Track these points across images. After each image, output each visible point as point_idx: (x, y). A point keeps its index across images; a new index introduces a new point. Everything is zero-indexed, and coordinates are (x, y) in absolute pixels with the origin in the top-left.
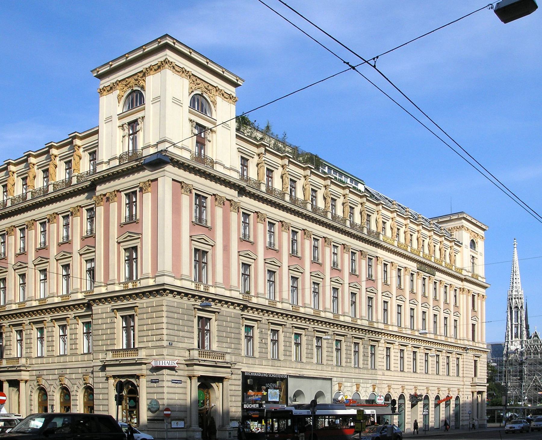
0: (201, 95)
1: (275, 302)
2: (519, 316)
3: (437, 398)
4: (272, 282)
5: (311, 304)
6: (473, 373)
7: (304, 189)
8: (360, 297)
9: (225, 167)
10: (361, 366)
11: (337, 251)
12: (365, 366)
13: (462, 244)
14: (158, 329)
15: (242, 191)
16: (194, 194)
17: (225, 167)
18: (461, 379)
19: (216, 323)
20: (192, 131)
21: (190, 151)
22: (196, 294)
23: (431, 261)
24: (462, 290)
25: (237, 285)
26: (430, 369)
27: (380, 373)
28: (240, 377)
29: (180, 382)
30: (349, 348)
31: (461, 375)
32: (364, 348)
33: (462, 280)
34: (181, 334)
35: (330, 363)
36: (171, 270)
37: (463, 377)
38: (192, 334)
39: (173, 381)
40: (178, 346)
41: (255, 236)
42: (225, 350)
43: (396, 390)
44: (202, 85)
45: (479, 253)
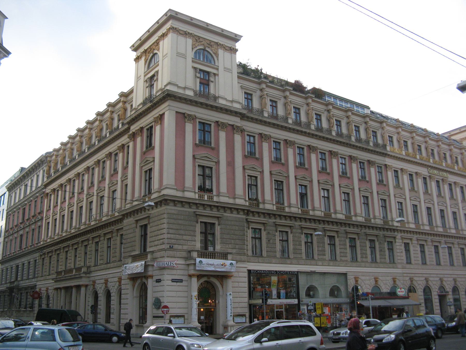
0: (204, 50)
1: (351, 217)
3: (442, 288)
7: (383, 137)
10: (378, 260)
12: (383, 260)
14: (152, 232)
15: (243, 117)
16: (198, 122)
19: (219, 227)
20: (196, 75)
21: (239, 103)
22: (197, 202)
24: (351, 158)
27: (399, 266)
28: (246, 274)
29: (181, 281)
32: (380, 243)
34: (185, 237)
35: (343, 259)
38: (194, 237)
39: (173, 281)
40: (179, 248)
42: (230, 251)
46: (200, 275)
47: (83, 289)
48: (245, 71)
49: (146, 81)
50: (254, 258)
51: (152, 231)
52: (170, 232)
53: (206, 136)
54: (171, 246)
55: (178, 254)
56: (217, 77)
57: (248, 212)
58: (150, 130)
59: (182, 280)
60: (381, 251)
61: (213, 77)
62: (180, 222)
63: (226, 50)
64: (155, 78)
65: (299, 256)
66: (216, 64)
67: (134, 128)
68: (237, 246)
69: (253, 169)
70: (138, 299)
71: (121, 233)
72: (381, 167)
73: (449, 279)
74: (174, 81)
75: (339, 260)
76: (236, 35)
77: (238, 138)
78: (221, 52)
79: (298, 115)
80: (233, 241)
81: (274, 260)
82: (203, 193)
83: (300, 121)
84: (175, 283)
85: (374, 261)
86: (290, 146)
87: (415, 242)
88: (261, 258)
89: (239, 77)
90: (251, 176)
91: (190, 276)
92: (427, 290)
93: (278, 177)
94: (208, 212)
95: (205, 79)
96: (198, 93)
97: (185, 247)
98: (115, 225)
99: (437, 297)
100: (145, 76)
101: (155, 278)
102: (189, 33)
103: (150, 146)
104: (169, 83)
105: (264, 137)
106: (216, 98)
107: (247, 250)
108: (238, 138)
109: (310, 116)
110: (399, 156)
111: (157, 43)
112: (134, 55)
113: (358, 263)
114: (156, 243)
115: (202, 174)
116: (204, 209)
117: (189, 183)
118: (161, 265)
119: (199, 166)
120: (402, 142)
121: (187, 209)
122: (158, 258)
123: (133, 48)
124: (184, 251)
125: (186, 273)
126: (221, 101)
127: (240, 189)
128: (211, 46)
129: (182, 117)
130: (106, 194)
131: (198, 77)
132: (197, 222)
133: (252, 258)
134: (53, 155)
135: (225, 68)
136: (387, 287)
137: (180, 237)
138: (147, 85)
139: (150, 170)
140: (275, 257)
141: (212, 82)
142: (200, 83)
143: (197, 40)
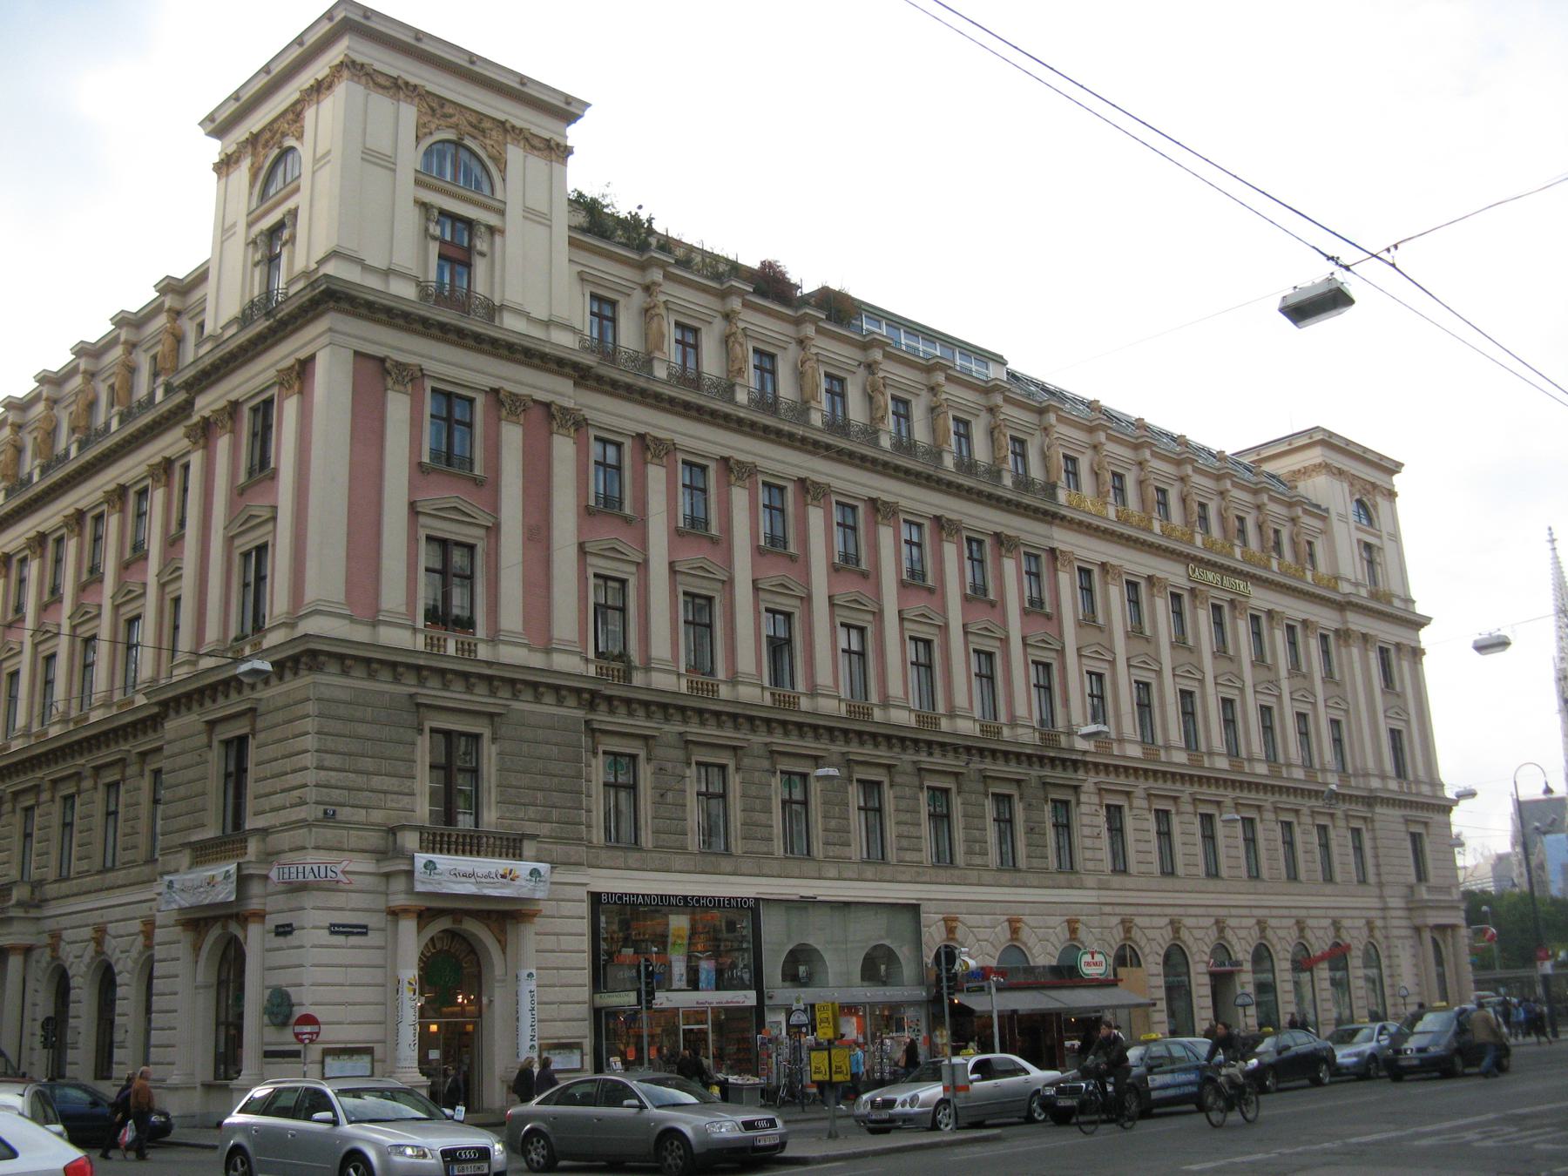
0: (458, 144)
4: (987, 678)
6: (1412, 870)
7: (1045, 457)
9: (366, 268)
10: (1022, 862)
11: (920, 534)
12: (1036, 863)
13: (1327, 510)
15: (582, 376)
17: (366, 268)
19: (494, 749)
21: (573, 329)
22: (422, 662)
25: (966, 705)
27: (1090, 881)
28: (584, 908)
29: (362, 930)
31: (1372, 878)
32: (1029, 807)
33: (1342, 606)
34: (376, 782)
35: (908, 856)
36: (341, 597)
38: (408, 782)
39: (335, 929)
40: (355, 818)
41: (804, 541)
42: (529, 828)
48: (595, 224)
49: (254, 242)
51: (266, 757)
52: (326, 764)
54: (330, 809)
55: (353, 838)
56: (498, 238)
57: (592, 699)
58: (265, 410)
59: (365, 927)
60: (1030, 831)
61: (486, 237)
62: (363, 729)
63: (533, 147)
64: (286, 235)
66: (499, 195)
67: (207, 403)
68: (555, 814)
69: (614, 553)
70: (213, 992)
74: (350, 246)
76: (569, 99)
77: (564, 448)
80: (539, 794)
81: (678, 861)
84: (341, 939)
85: (1009, 863)
87: (1139, 802)
88: (637, 855)
89: (572, 242)
90: (606, 578)
91: (395, 914)
92: (1175, 959)
94: (456, 695)
95: (459, 244)
96: (432, 290)
97: (377, 816)
99: (1206, 979)
100: (250, 225)
102: (407, 84)
103: (261, 467)
104: (334, 254)
105: (652, 446)
106: (492, 311)
107: (589, 826)
108: (564, 448)
110: (1096, 522)
111: (295, 113)
112: (214, 149)
113: (957, 872)
115: (438, 566)
116: (446, 687)
117: (393, 596)
118: (293, 875)
119: (429, 538)
120: (1108, 477)
121: (384, 685)
122: (284, 852)
125: (381, 903)
127: (566, 619)
128: (483, 131)
129: (376, 372)
130: (105, 632)
131: (434, 238)
132: (420, 731)
133: (604, 855)
135: (527, 210)
136: (1050, 948)
137: (360, 780)
139: (262, 550)
140: (683, 850)
141: (482, 254)
142: (441, 256)
143: (433, 110)
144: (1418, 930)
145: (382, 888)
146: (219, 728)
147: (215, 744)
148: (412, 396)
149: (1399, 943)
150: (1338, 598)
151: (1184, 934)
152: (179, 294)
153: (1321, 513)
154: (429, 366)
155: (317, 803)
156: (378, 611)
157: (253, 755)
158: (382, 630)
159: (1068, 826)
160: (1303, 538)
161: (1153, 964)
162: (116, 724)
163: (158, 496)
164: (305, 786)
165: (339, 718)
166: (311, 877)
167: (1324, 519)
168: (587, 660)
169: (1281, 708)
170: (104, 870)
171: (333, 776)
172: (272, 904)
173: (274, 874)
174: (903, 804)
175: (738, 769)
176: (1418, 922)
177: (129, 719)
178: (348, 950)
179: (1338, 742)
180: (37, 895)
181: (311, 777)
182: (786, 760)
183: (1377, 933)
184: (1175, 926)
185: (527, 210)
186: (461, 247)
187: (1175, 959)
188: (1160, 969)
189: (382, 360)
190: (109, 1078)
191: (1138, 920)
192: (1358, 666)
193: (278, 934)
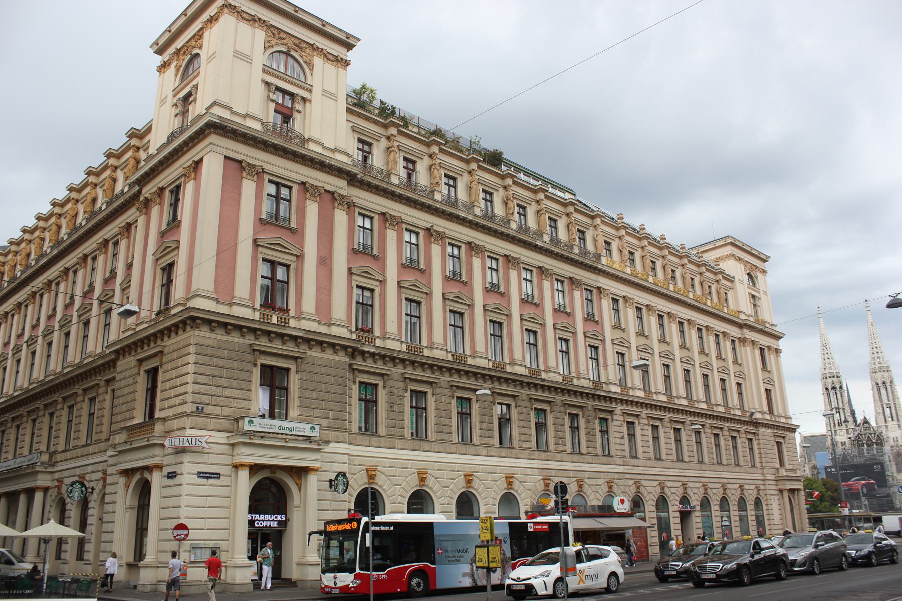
1: (538, 372)
2: (890, 394)
4: (497, 337)
5: (588, 374)
6: (778, 461)
7: (595, 241)
8: (713, 379)
10: (584, 450)
11: (532, 276)
12: (591, 450)
15: (352, 179)
18: (760, 471)
19: (297, 377)
20: (268, 96)
22: (257, 326)
23: (648, 282)
26: (741, 459)
29: (217, 476)
30: (560, 421)
31: (758, 465)
32: (587, 421)
33: (741, 326)
34: (228, 392)
35: (525, 445)
36: (212, 289)
37: (762, 468)
38: (247, 393)
39: (201, 475)
40: (215, 412)
43: (650, 490)
44: (290, 41)
45: (761, 293)
46: (256, 465)
47: (38, 496)
48: (359, 103)
49: (176, 105)
50: (362, 437)
51: (167, 378)
52: (199, 381)
53: (282, 207)
54: (200, 406)
55: (212, 423)
56: (307, 104)
57: (354, 352)
58: (177, 191)
59: (219, 474)
60: (588, 434)
61: (302, 103)
62: (221, 362)
63: (329, 59)
64: (192, 99)
65: (446, 437)
67: (148, 190)
68: (331, 414)
69: (367, 275)
70: (135, 513)
71: (112, 387)
72: (591, 291)
73: (697, 485)
74: (223, 99)
75: (517, 447)
76: (348, 36)
77: (340, 217)
78: (318, 61)
79: (452, 189)
80: (323, 403)
81: (399, 443)
82: (269, 312)
83: (456, 199)
84: (204, 481)
85: (576, 451)
86: (436, 240)
88: (376, 439)
89: (349, 111)
91: (236, 467)
92: (662, 503)
93: (413, 293)
94: (277, 346)
96: (270, 127)
97: (227, 411)
98: (104, 372)
99: (678, 514)
100: (175, 96)
101: (166, 470)
102: (259, 19)
103: (174, 223)
104: (215, 104)
105: (390, 219)
106: (304, 141)
107: (350, 422)
108: (340, 217)
109: (473, 191)
110: (621, 275)
111: (199, 35)
112: (158, 60)
113: (549, 454)
114: (171, 402)
115: (269, 276)
117: (242, 290)
118: (177, 444)
119: (264, 260)
120: (627, 253)
121: (235, 338)
122: (174, 431)
123: (156, 47)
124: (224, 417)
125: (228, 460)
126: (312, 146)
127: (340, 308)
128: (301, 48)
129: (237, 168)
131: (273, 101)
132: (255, 365)
133: (358, 438)
134: (9, 252)
135: (324, 90)
136: (598, 496)
137: (218, 391)
138: (178, 111)
139: (171, 266)
140: (402, 437)
141: (299, 112)
142: (276, 111)
143: (274, 34)
144: (781, 491)
145: (230, 452)
146: (144, 364)
147: (142, 372)
148: (257, 183)
149: (772, 497)
150: (740, 321)
151: (667, 490)
152: (138, 135)
153: (731, 280)
154: (267, 167)
155: (193, 402)
156: (233, 298)
157: (161, 377)
158: (235, 307)
159: (607, 432)
160: (722, 291)
161: (650, 506)
162: (94, 365)
163: (123, 244)
164: (187, 393)
165: (208, 355)
166: (187, 445)
167: (732, 282)
168: (351, 331)
169: (713, 376)
170: (87, 445)
171: (203, 388)
172: (166, 461)
173: (166, 443)
174: (522, 417)
175: (433, 394)
176: (781, 487)
177: (101, 362)
178: (208, 487)
179: (740, 394)
180: (53, 460)
181: (190, 388)
182: (460, 391)
183: (761, 492)
184: (662, 485)
185: (324, 90)
186: (287, 107)
187: (662, 503)
188: (654, 509)
189: (240, 162)
190: (82, 560)
191: (643, 483)
192: (749, 355)
193: (169, 477)
